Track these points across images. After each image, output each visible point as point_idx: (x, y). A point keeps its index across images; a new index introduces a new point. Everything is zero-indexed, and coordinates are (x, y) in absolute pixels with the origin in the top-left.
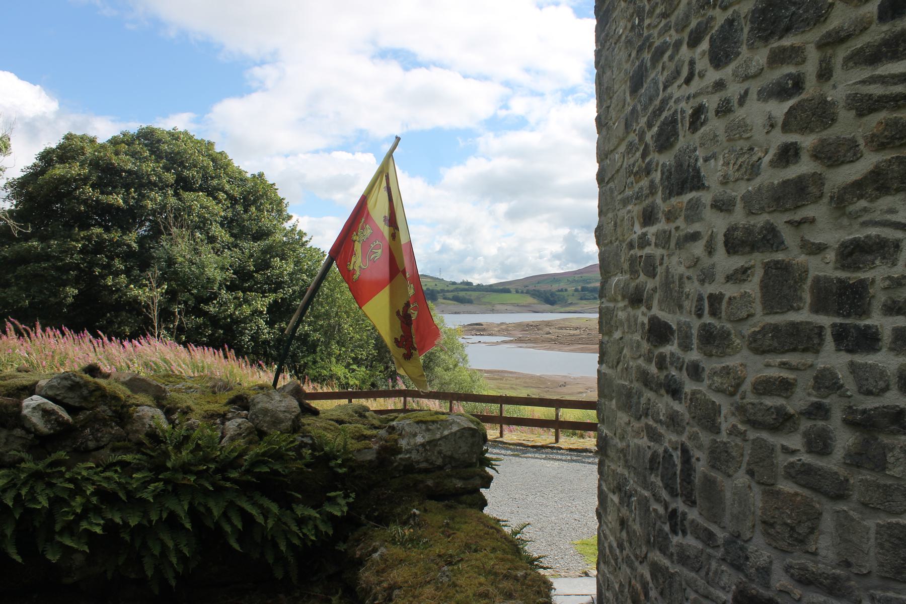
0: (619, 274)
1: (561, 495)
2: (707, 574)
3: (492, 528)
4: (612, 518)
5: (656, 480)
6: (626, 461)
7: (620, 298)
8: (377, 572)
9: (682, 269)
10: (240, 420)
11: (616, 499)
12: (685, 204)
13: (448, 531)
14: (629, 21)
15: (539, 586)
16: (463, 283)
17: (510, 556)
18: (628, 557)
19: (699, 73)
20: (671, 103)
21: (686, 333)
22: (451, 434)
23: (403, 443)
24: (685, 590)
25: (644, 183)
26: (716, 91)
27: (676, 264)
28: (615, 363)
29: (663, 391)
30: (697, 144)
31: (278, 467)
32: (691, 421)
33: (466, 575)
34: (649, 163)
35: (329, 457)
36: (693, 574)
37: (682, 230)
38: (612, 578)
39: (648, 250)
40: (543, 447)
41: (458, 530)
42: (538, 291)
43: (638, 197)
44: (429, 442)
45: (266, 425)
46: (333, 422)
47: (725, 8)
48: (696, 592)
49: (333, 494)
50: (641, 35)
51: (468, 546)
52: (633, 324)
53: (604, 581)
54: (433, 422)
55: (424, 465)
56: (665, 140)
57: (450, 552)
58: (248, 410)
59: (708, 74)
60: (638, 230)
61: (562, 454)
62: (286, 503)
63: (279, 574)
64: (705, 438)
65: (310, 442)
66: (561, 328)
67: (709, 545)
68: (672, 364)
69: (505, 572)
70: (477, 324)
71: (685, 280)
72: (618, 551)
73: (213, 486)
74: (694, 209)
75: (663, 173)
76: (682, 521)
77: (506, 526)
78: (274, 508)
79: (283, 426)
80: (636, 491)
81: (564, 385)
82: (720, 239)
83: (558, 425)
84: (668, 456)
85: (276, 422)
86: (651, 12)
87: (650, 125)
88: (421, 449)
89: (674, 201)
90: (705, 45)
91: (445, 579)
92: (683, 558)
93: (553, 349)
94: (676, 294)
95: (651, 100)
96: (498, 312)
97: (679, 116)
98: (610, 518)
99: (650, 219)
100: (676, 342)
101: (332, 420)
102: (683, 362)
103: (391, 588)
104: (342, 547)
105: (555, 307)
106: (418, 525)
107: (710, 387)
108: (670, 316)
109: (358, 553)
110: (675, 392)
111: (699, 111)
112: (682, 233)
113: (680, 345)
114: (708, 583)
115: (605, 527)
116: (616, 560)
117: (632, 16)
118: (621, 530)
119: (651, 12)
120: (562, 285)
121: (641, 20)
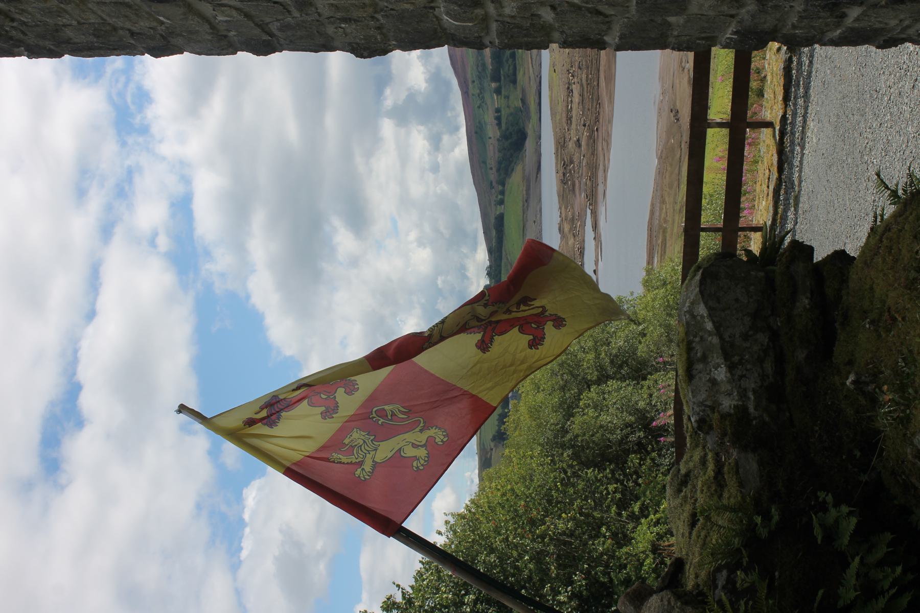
0: (437, 12)
1: (870, 116)
3: (881, 241)
7: (479, 11)
22: (710, 316)
23: (727, 404)
28: (601, 18)
40: (781, 151)
42: (500, 163)
44: (726, 356)
46: (694, 533)
49: (818, 533)
55: (769, 366)
61: (794, 114)
66: (569, 119)
77: (882, 216)
81: (675, 112)
83: (740, 124)
88: (738, 372)
93: (609, 135)
98: (893, 23)
101: (690, 533)
105: (530, 131)
120: (489, 118)
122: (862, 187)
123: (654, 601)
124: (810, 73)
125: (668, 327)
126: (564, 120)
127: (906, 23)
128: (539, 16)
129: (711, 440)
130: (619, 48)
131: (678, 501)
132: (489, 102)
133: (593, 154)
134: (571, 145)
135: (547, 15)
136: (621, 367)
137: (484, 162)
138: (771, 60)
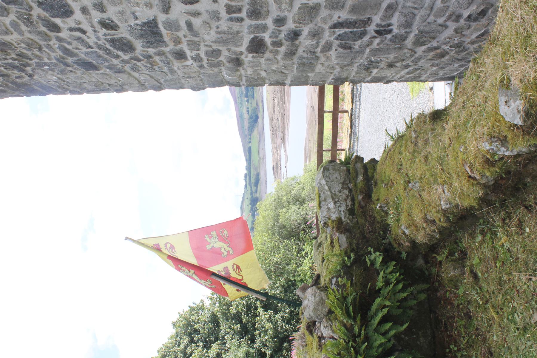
0: (222, 74)
2: (416, 8)
4: (388, 73)
5: (357, 45)
6: (348, 65)
7: (238, 73)
8: (417, 231)
9: (213, 32)
10: (322, 327)
11: (375, 71)
12: (168, 32)
13: (390, 184)
14: (47, 72)
15: (421, 122)
16: (245, 180)
17: (404, 142)
18: (413, 61)
19: (78, 25)
20: (100, 43)
21: (255, 28)
23: (334, 217)
24: (429, 23)
25: (157, 59)
26: (89, 13)
27: (209, 36)
28: (283, 75)
29: (297, 42)
30: (127, 24)
31: (349, 300)
32: (314, 23)
33: (415, 171)
34: (144, 56)
35: (344, 265)
36: (418, 18)
37: (186, 33)
38: (429, 72)
39: (203, 55)
41: (389, 177)
42: (249, 128)
43: (168, 63)
44: (333, 199)
45: (324, 309)
47: (31, 8)
48: (429, 15)
49: (368, 262)
50: (56, 65)
51: (399, 170)
52: (254, 64)
53: (433, 77)
54: (320, 197)
55: (349, 202)
56: (126, 46)
57: (402, 182)
58: (316, 322)
59: (77, 19)
60: (190, 62)
61: (356, 108)
62: (377, 293)
63: (423, 296)
64: (324, 13)
65: (335, 279)
66: (274, 111)
67: (396, 8)
68: (277, 37)
69: (413, 145)
70: (273, 169)
71: (219, 30)
72: (411, 68)
73: (364, 343)
74: (169, 25)
75: (149, 47)
76: (382, 27)
78: (378, 301)
79: (324, 297)
80: (368, 58)
82: (189, 7)
84: (340, 37)
85: (322, 302)
86: (39, 58)
87: (117, 57)
88: (338, 204)
89: (166, 39)
90: (58, 21)
91: (418, 185)
92: (408, 25)
93: (289, 116)
94: (230, 36)
95: (100, 56)
96: (264, 155)
97: (108, 37)
99: (182, 55)
100: (262, 35)
102: (275, 29)
103: (426, 221)
104: (404, 255)
105: (260, 116)
106: (387, 204)
107: (289, 11)
108: (245, 39)
109: (407, 244)
110: (295, 35)
111: (104, 24)
112: (188, 33)
113: (264, 32)
114: (422, 8)
115: (396, 78)
116: (417, 70)
117: (44, 71)
118: (396, 66)
119: (39, 58)
120: (245, 111)
121: (46, 64)
122: (381, 134)
123: (309, 290)
124: (361, 93)
125: (313, 187)
127: (393, 75)
128: (260, 74)
129: (329, 230)
130: (290, 85)
131: (318, 253)
132: (244, 105)
133: (283, 123)
134: (275, 120)
135: (263, 74)
136: (296, 202)
137: (243, 127)
138: (346, 88)
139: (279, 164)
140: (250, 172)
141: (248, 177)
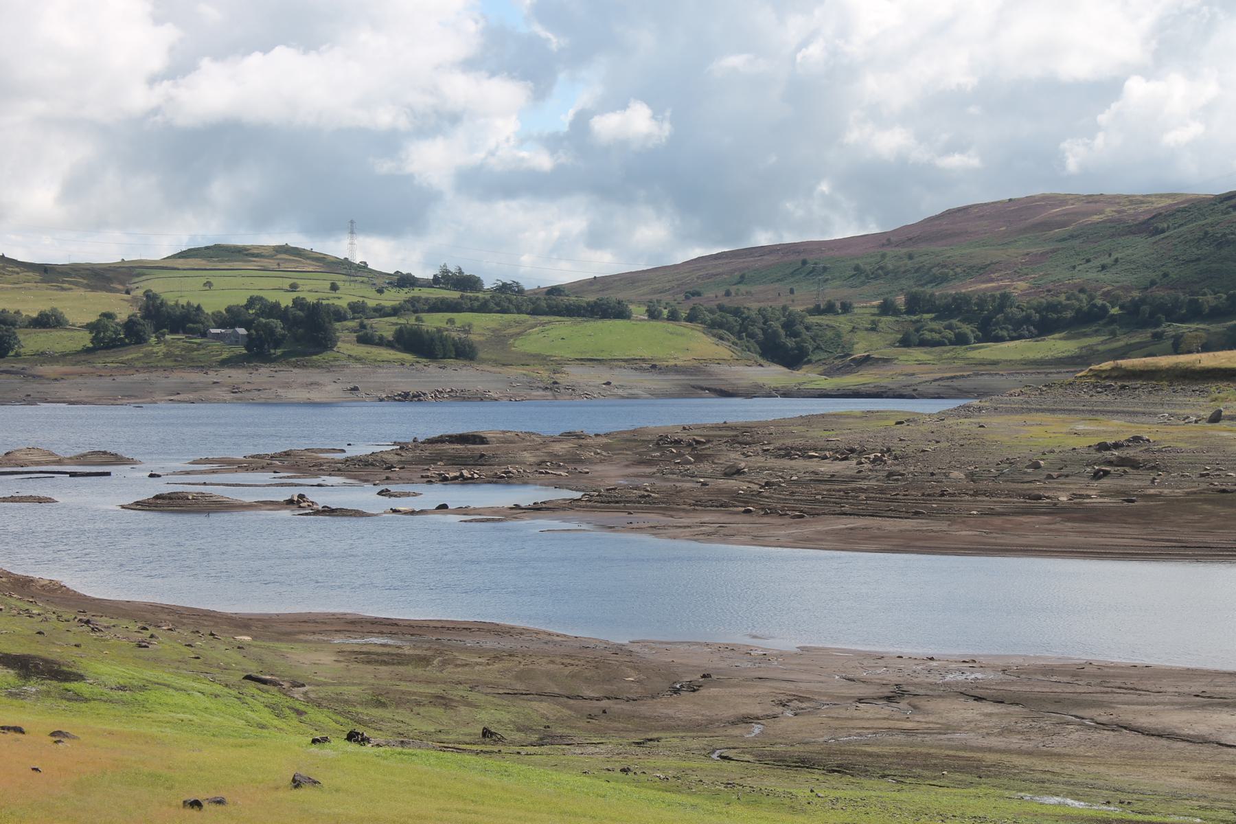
16: (446, 279)
42: (736, 312)
120: (834, 292)
126: (789, 442)
133: (698, 503)
139: (486, 471)
140: (483, 308)
141: (454, 295)
